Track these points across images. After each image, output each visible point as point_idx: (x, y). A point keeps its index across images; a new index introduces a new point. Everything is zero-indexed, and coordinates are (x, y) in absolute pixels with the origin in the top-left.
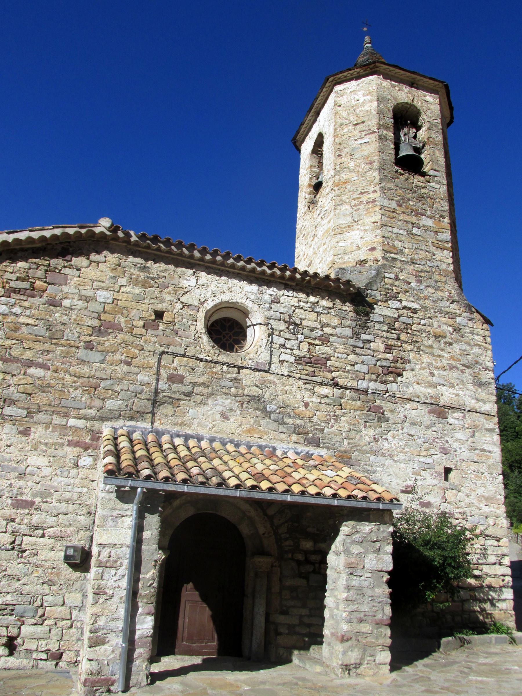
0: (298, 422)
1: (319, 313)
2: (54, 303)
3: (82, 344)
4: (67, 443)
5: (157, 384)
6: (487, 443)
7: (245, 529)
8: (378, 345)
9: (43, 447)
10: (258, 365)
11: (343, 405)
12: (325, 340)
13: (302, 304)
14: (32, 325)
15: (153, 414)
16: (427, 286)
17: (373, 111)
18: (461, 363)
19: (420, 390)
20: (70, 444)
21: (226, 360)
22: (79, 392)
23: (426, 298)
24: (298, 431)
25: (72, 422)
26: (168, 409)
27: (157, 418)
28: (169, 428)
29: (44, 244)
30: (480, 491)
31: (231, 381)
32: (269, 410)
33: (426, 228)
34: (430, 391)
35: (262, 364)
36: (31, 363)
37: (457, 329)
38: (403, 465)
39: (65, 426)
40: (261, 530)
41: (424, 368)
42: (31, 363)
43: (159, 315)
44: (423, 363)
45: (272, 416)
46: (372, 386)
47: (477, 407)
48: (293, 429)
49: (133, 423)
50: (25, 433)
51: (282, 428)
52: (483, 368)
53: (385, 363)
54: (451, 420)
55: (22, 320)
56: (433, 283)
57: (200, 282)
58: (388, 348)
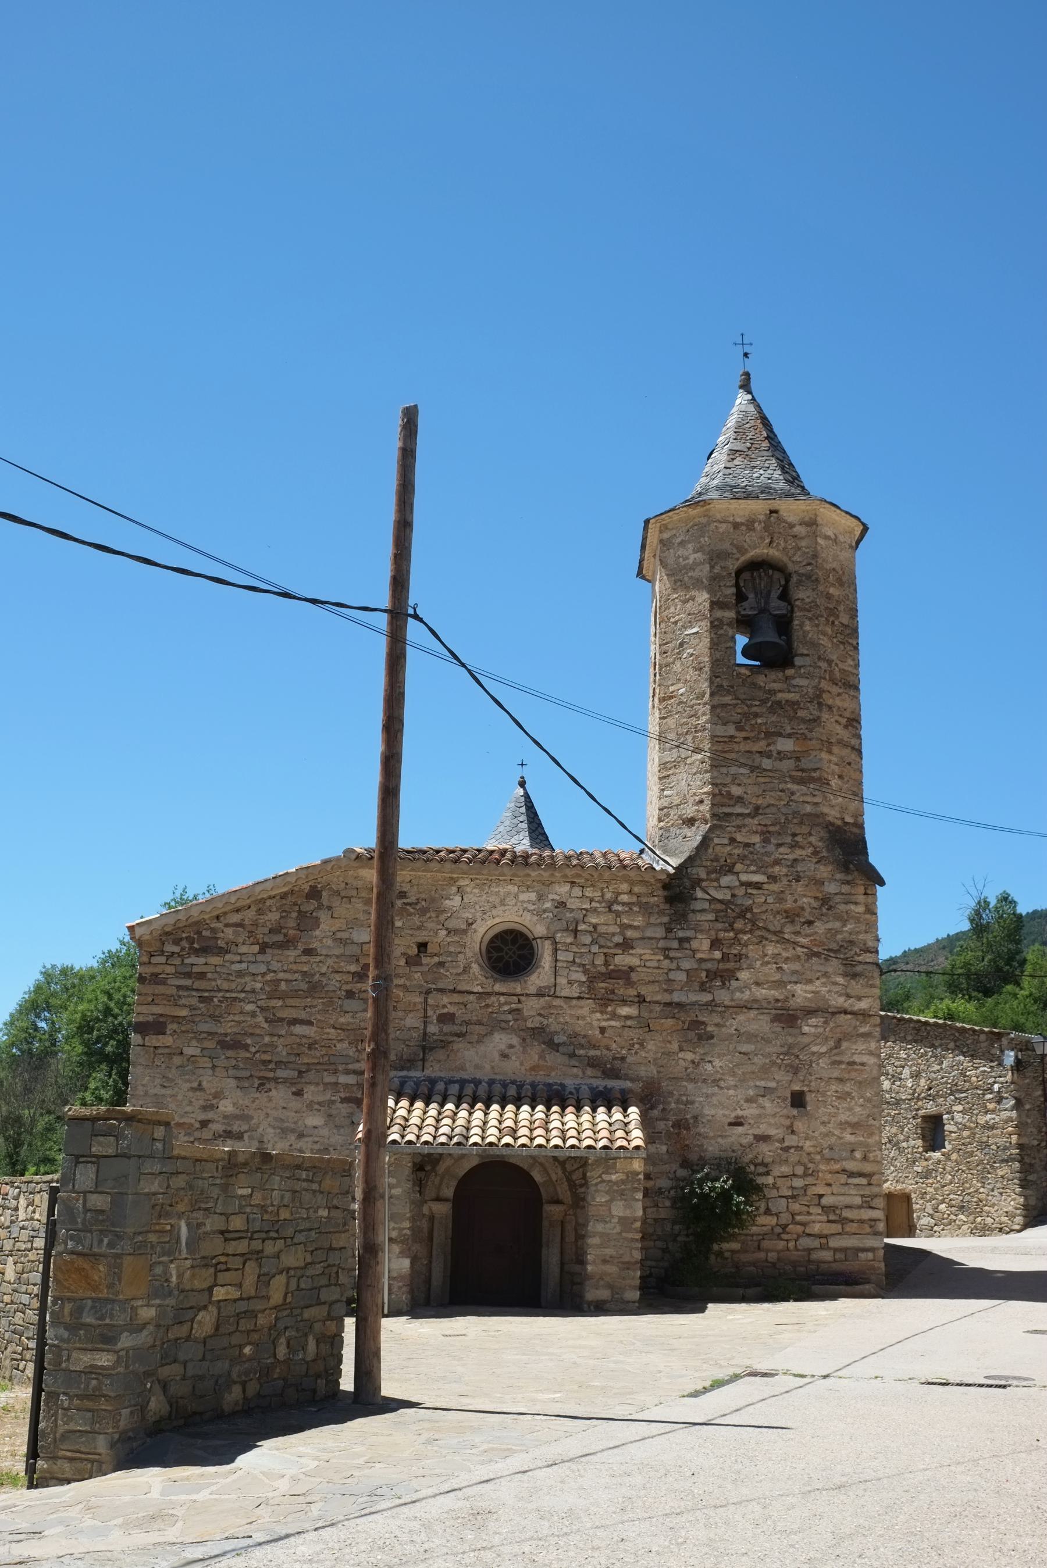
0: (592, 1053)
1: (618, 914)
2: (308, 952)
3: (344, 993)
4: (339, 1100)
5: (425, 1027)
6: (859, 1054)
7: (537, 1176)
8: (701, 944)
9: (316, 1107)
10: (541, 990)
11: (651, 1025)
12: (626, 945)
13: (594, 904)
14: (291, 981)
15: (423, 1060)
16: (779, 845)
17: (704, 580)
18: (826, 947)
19: (762, 993)
20: (344, 1100)
21: (503, 990)
22: (345, 1045)
23: (777, 862)
24: (593, 1063)
25: (343, 1079)
26: (441, 1054)
27: (427, 1064)
28: (442, 1075)
29: (290, 887)
30: (843, 1117)
31: (510, 1013)
32: (556, 1041)
33: (781, 756)
34: (775, 993)
35: (545, 987)
36: (294, 1022)
37: (825, 901)
38: (731, 1092)
39: (336, 1084)
40: (554, 1177)
41: (768, 963)
42: (294, 1022)
43: (422, 946)
44: (766, 955)
45: (560, 1048)
46: (693, 997)
47: (846, 1005)
48: (586, 1062)
49: (404, 1073)
50: (299, 1093)
51: (574, 1062)
52: (861, 950)
53: (709, 965)
54: (806, 1029)
55: (281, 975)
56: (789, 839)
57: (466, 900)
58: (715, 944)
